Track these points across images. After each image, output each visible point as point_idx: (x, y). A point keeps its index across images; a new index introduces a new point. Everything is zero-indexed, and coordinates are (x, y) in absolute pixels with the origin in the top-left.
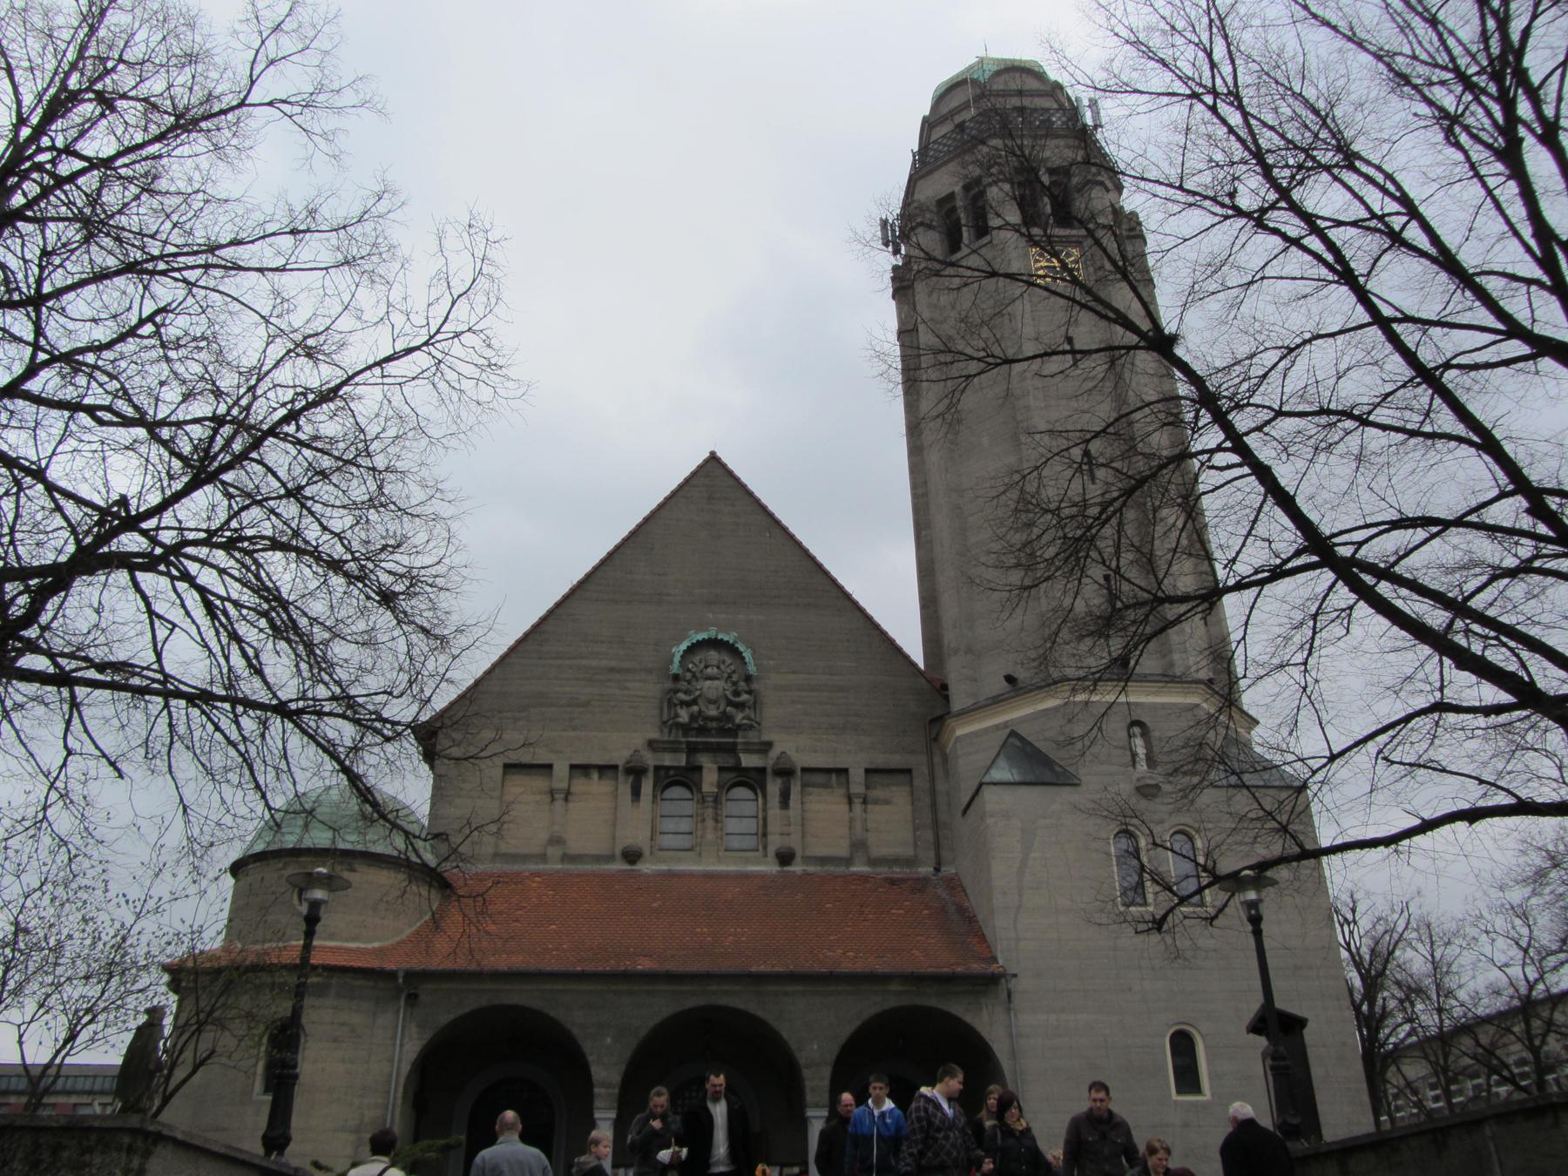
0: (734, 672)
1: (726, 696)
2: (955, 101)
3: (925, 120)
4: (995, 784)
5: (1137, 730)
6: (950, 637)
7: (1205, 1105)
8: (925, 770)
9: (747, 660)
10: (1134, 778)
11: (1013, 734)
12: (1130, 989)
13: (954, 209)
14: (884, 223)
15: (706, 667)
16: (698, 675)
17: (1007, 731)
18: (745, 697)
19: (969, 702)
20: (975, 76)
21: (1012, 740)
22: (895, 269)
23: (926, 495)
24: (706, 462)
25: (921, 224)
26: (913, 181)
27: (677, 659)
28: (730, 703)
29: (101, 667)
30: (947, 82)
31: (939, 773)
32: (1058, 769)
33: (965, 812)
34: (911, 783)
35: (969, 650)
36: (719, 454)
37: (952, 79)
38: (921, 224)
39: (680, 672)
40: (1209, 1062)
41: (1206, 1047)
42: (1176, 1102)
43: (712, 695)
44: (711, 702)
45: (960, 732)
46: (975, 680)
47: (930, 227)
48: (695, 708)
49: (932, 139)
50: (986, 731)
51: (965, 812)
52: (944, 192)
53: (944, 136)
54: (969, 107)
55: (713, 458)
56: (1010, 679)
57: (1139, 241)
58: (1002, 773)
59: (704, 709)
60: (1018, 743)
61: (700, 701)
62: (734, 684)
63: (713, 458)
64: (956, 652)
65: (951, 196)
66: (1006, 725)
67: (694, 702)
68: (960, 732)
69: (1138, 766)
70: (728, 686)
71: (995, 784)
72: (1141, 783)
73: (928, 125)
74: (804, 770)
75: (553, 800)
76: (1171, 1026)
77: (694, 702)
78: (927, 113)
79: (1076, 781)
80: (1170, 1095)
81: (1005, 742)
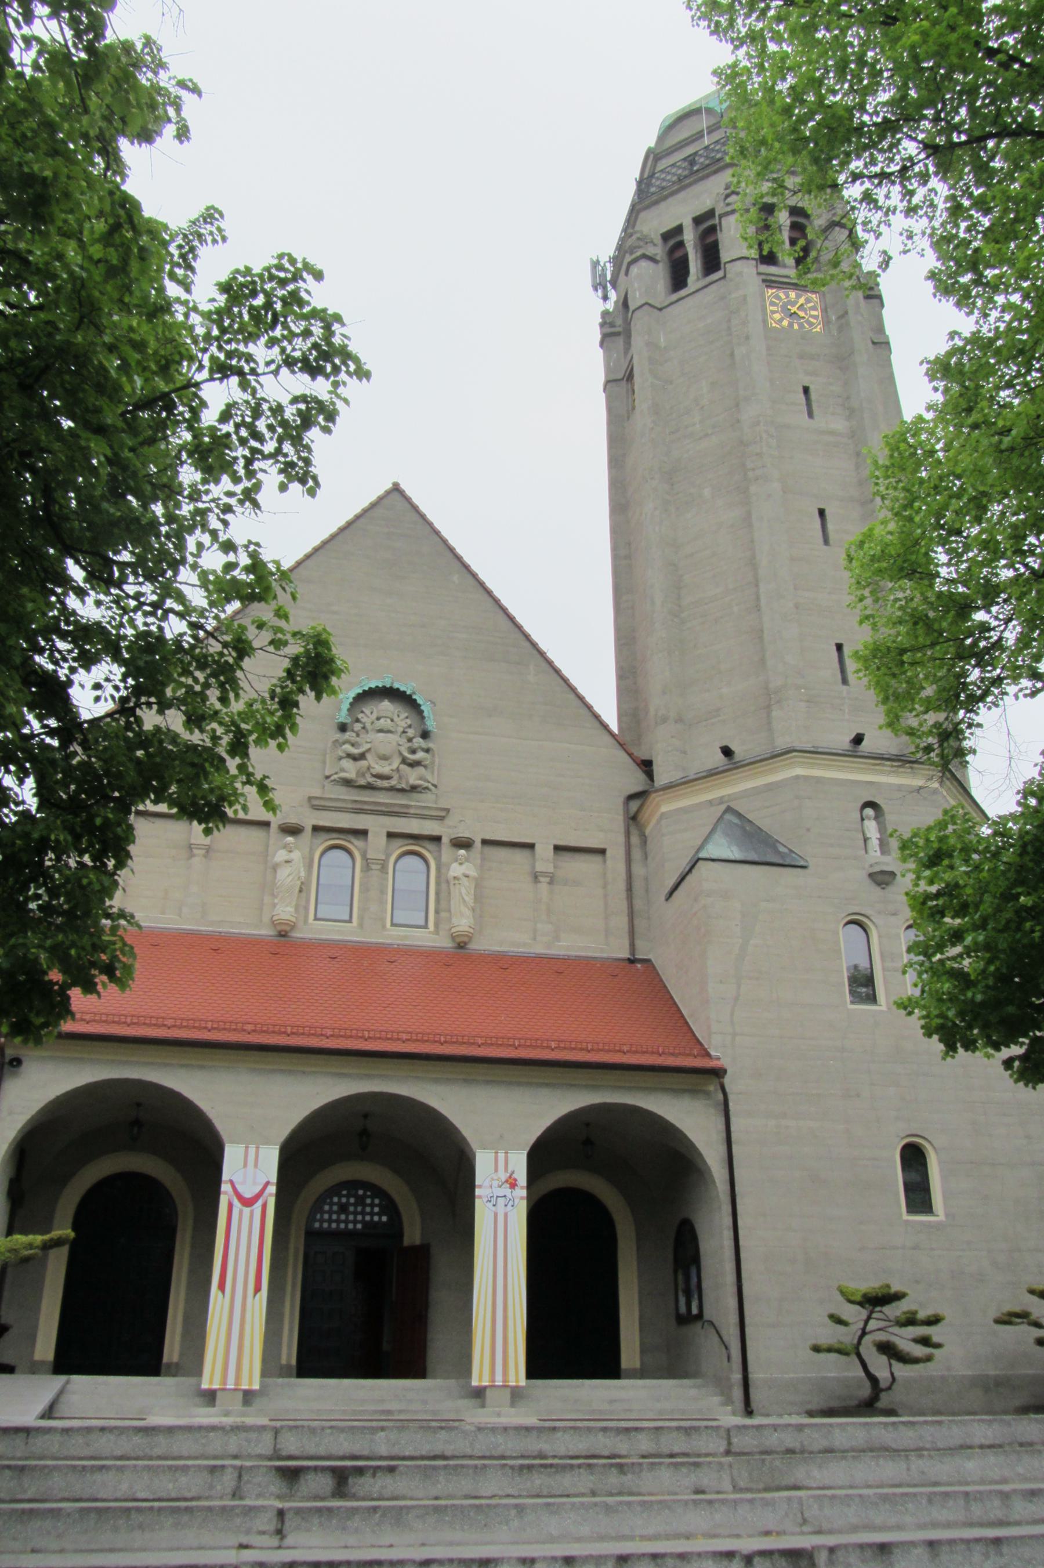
0: (410, 726)
1: (400, 754)
2: (684, 133)
3: (649, 152)
4: (713, 860)
5: (869, 812)
6: (656, 703)
7: (938, 1226)
8: (621, 852)
9: (426, 714)
10: (867, 866)
11: (729, 810)
12: (858, 1095)
13: (681, 244)
14: (595, 264)
15: (378, 719)
16: (368, 726)
17: (723, 807)
18: (420, 755)
19: (676, 776)
20: (711, 105)
21: (728, 817)
22: (605, 314)
23: (628, 557)
24: (388, 493)
25: (645, 256)
26: (634, 212)
27: (346, 706)
28: (404, 761)
29: (185, 1469)
30: (677, 112)
31: (637, 854)
32: (782, 849)
33: (671, 894)
34: (605, 861)
35: (679, 720)
36: (403, 486)
37: (683, 109)
38: (645, 256)
39: (348, 721)
40: (944, 1178)
41: (940, 1162)
42: (907, 1221)
43: (383, 750)
44: (384, 758)
45: (664, 809)
46: (685, 753)
47: (652, 259)
48: (363, 763)
49: (659, 168)
50: (698, 806)
51: (671, 894)
52: (670, 225)
53: (673, 165)
54: (703, 136)
55: (396, 488)
56: (727, 752)
57: (876, 301)
58: (721, 847)
59: (373, 765)
60: (736, 821)
61: (368, 756)
62: (410, 740)
63: (396, 488)
64: (665, 720)
65: (679, 230)
66: (721, 800)
67: (362, 756)
68: (664, 809)
69: (870, 851)
70: (403, 741)
71: (713, 860)
72: (877, 869)
73: (653, 157)
74: (485, 842)
75: (192, 856)
76: (902, 1138)
77: (362, 756)
78: (652, 145)
79: (802, 863)
80: (901, 1214)
81: (721, 817)
